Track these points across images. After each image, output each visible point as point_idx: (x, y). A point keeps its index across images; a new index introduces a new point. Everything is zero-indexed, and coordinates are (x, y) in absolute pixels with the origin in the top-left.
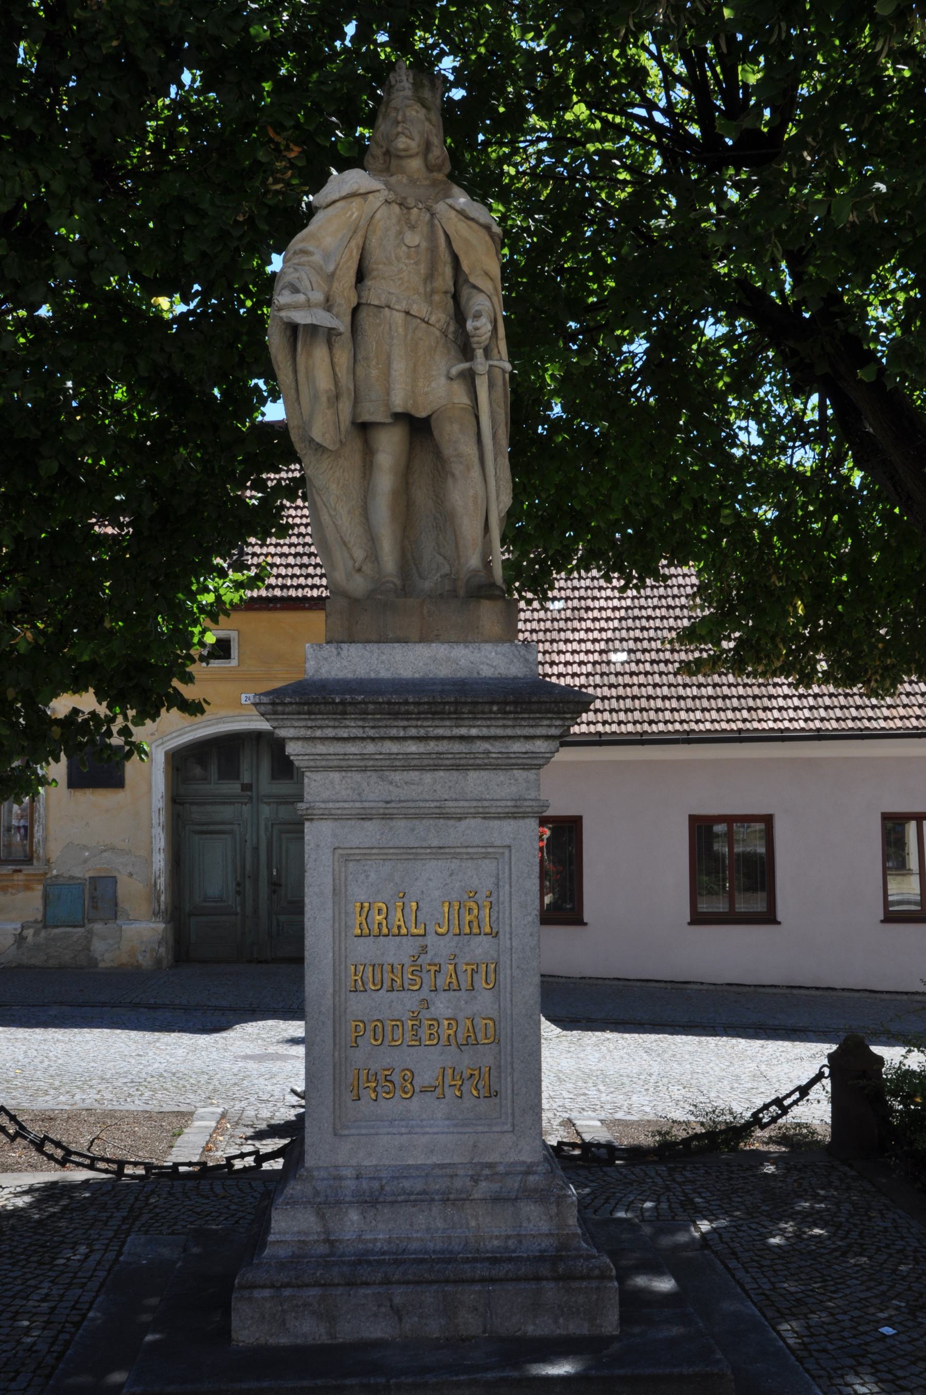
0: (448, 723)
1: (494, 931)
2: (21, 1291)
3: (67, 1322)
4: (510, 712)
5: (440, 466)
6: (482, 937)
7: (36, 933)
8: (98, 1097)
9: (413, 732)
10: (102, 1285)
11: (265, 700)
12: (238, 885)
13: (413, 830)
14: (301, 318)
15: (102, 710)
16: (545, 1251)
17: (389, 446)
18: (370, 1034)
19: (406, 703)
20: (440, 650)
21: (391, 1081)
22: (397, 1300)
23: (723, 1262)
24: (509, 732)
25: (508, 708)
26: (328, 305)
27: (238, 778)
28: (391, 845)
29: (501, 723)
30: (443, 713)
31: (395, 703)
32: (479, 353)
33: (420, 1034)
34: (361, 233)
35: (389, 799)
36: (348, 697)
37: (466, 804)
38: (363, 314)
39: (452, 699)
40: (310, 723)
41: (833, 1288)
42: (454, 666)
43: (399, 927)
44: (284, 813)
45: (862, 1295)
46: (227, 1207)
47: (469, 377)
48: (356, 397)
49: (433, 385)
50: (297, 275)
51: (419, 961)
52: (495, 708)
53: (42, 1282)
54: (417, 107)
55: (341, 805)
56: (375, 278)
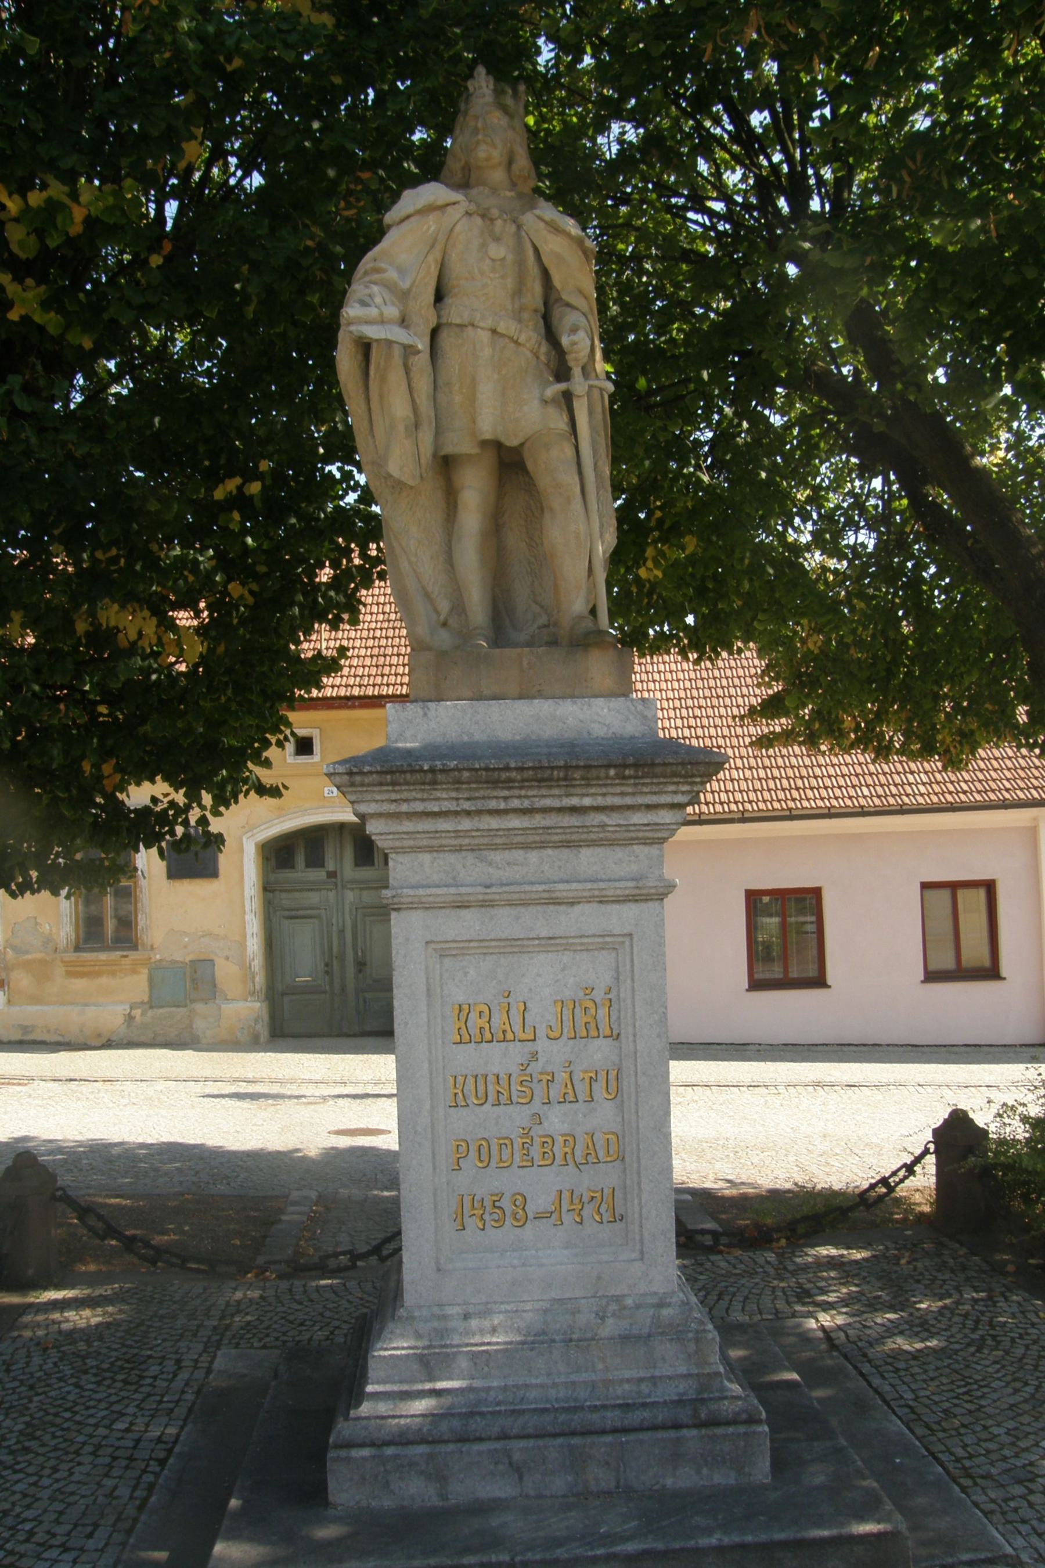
0: (556, 791)
1: (615, 1033)
2: (103, 1418)
3: (151, 1458)
4: (630, 777)
6: (601, 1041)
7: (143, 1014)
8: (195, 1179)
9: (516, 803)
10: (190, 1410)
11: (341, 769)
12: (327, 965)
13: (518, 918)
14: (372, 332)
15: (180, 797)
16: (684, 1394)
17: (474, 489)
18: (473, 1153)
19: (507, 768)
20: (543, 707)
21: (500, 1208)
22: (517, 1457)
23: (855, 1367)
24: (628, 800)
25: (627, 772)
26: (403, 322)
27: (322, 866)
28: (492, 937)
29: (618, 790)
30: (550, 779)
31: (494, 769)
32: (577, 372)
33: (532, 1153)
34: (438, 247)
35: (488, 882)
36: (438, 763)
37: (580, 886)
38: (444, 336)
39: (562, 763)
40: (394, 796)
41: (979, 1394)
42: (560, 725)
43: (504, 1032)
44: (368, 897)
45: (1012, 1400)
46: (321, 1314)
47: (568, 397)
48: (437, 427)
49: (526, 409)
50: (367, 291)
51: (529, 1070)
52: (612, 772)
53: (127, 1406)
55: (434, 891)
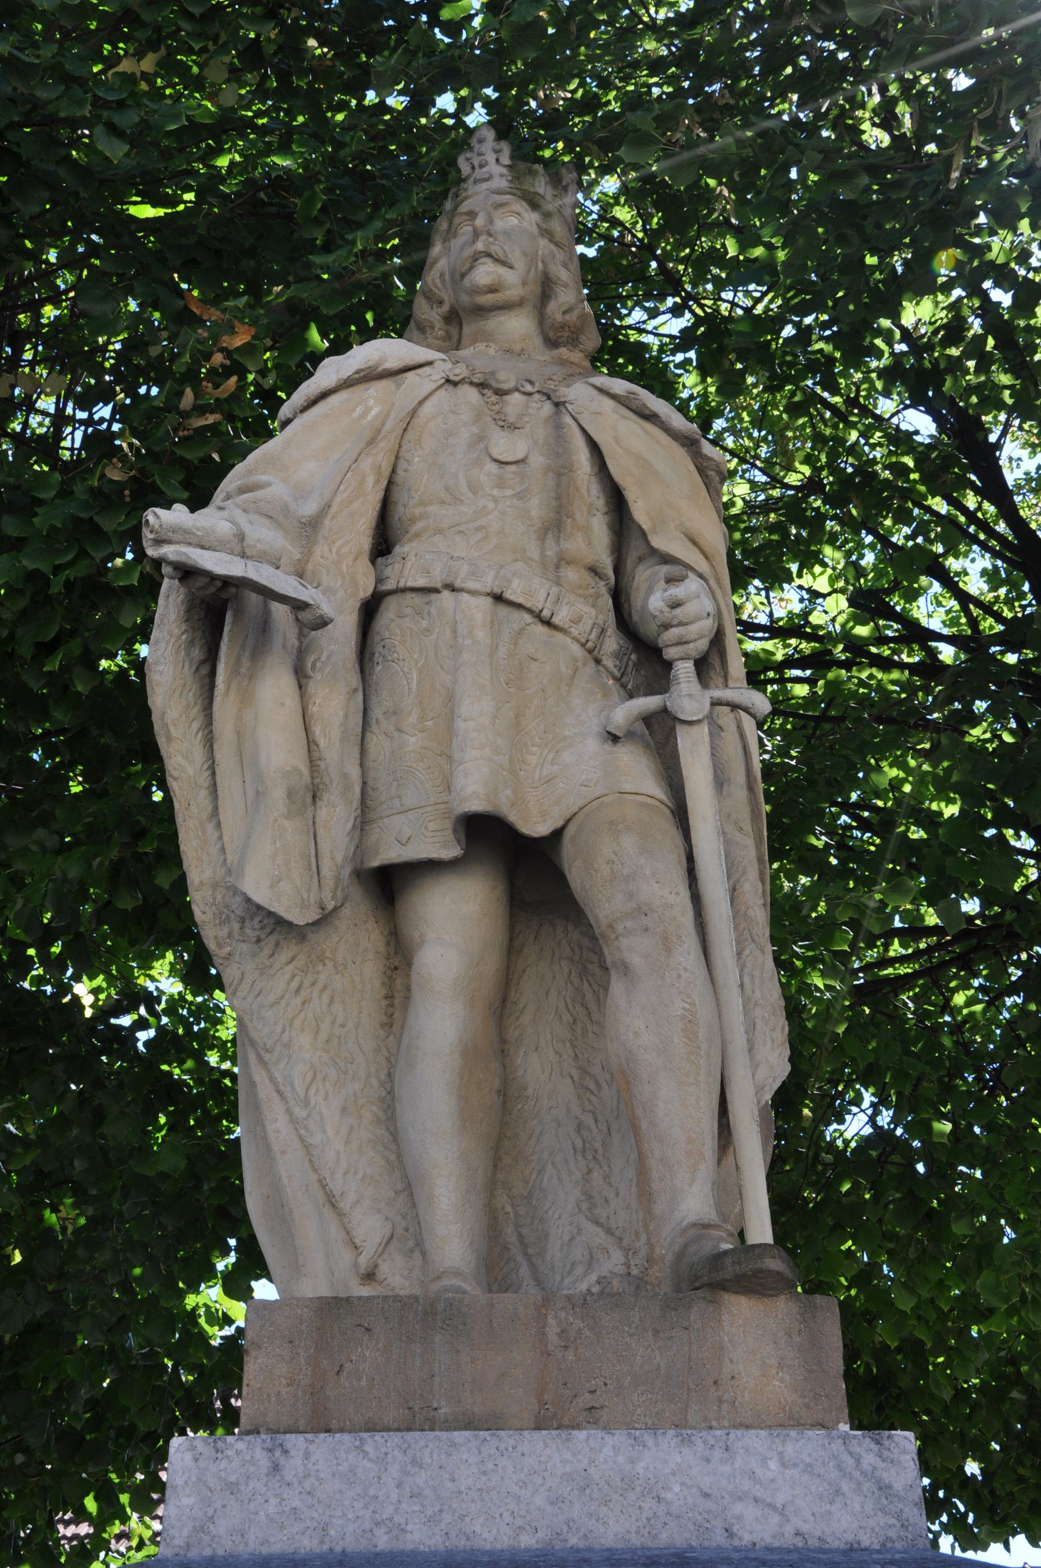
5: (592, 961)
17: (456, 921)
20: (599, 1452)
32: (684, 670)
42: (648, 1504)
47: (659, 733)
49: (567, 757)
54: (520, 206)
56: (417, 535)
